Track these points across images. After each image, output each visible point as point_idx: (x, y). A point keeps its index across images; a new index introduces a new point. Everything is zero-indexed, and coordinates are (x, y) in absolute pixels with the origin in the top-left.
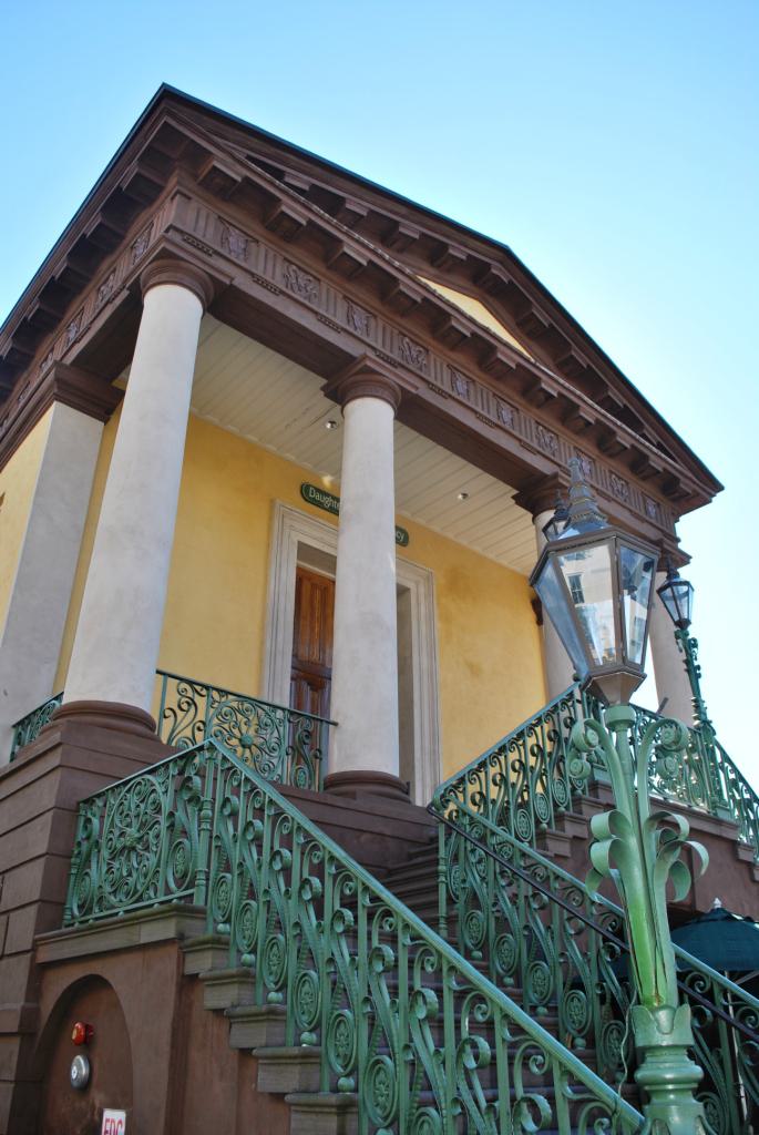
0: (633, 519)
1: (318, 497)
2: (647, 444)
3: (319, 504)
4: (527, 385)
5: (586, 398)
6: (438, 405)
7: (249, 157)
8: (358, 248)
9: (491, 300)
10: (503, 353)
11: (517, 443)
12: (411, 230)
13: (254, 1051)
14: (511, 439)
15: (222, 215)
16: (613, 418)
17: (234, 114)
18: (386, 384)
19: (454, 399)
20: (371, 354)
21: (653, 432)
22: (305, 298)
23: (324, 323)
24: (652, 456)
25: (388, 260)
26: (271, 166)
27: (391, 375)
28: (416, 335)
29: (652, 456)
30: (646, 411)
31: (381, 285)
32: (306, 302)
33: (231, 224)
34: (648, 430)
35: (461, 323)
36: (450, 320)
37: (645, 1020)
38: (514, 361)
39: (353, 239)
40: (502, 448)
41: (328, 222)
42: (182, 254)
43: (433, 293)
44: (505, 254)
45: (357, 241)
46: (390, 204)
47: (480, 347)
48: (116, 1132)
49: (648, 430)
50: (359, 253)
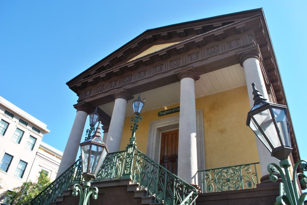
2: (220, 28)
6: (135, 86)
7: (84, 78)
8: (102, 75)
10: (144, 60)
13: (305, 178)
17: (72, 79)
20: (237, 50)
22: (172, 68)
25: (109, 71)
26: (87, 76)
32: (173, 68)
33: (230, 41)
34: (215, 24)
35: (130, 65)
37: (49, 180)
41: (96, 76)
42: (242, 52)
43: (133, 61)
44: (148, 32)
45: (103, 73)
46: (112, 56)
47: (170, 52)
48: (78, 199)
49: (215, 24)
50: (146, 59)
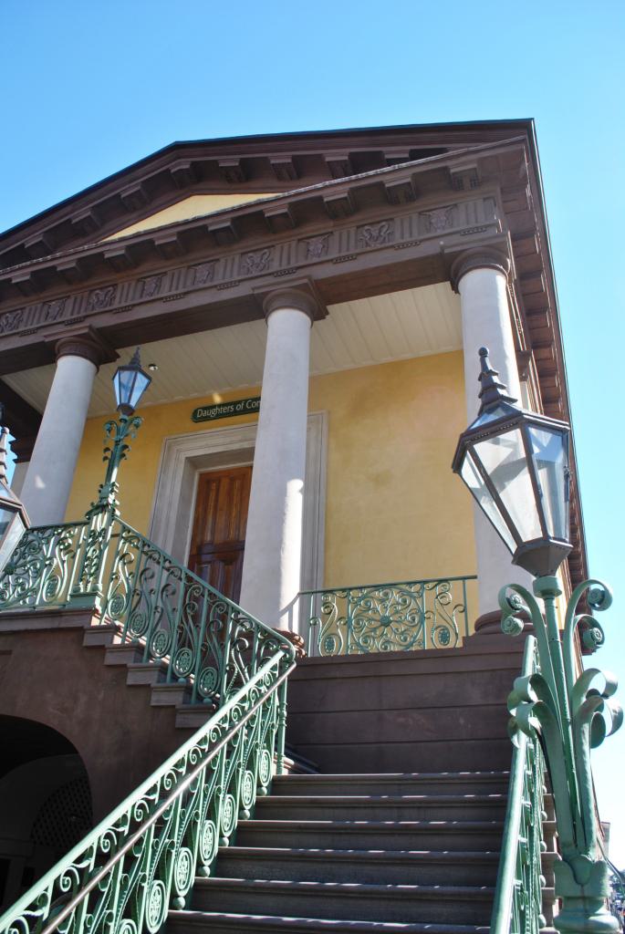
0: (23, 338)
1: (205, 413)
3: (207, 419)
4: (303, 213)
5: (302, 190)
9: (201, 186)
10: (159, 238)
11: (331, 264)
12: (83, 213)
14: (266, 278)
15: (299, 237)
16: (307, 188)
18: (65, 343)
19: (134, 305)
21: (393, 148)
23: (177, 299)
24: (448, 163)
25: (42, 263)
27: (62, 333)
28: (101, 283)
29: (448, 163)
30: (381, 138)
31: (94, 267)
36: (384, 185)
38: (172, 235)
39: (17, 270)
40: (356, 272)
44: (178, 149)
45: (20, 269)
46: (46, 221)
49: (390, 152)
